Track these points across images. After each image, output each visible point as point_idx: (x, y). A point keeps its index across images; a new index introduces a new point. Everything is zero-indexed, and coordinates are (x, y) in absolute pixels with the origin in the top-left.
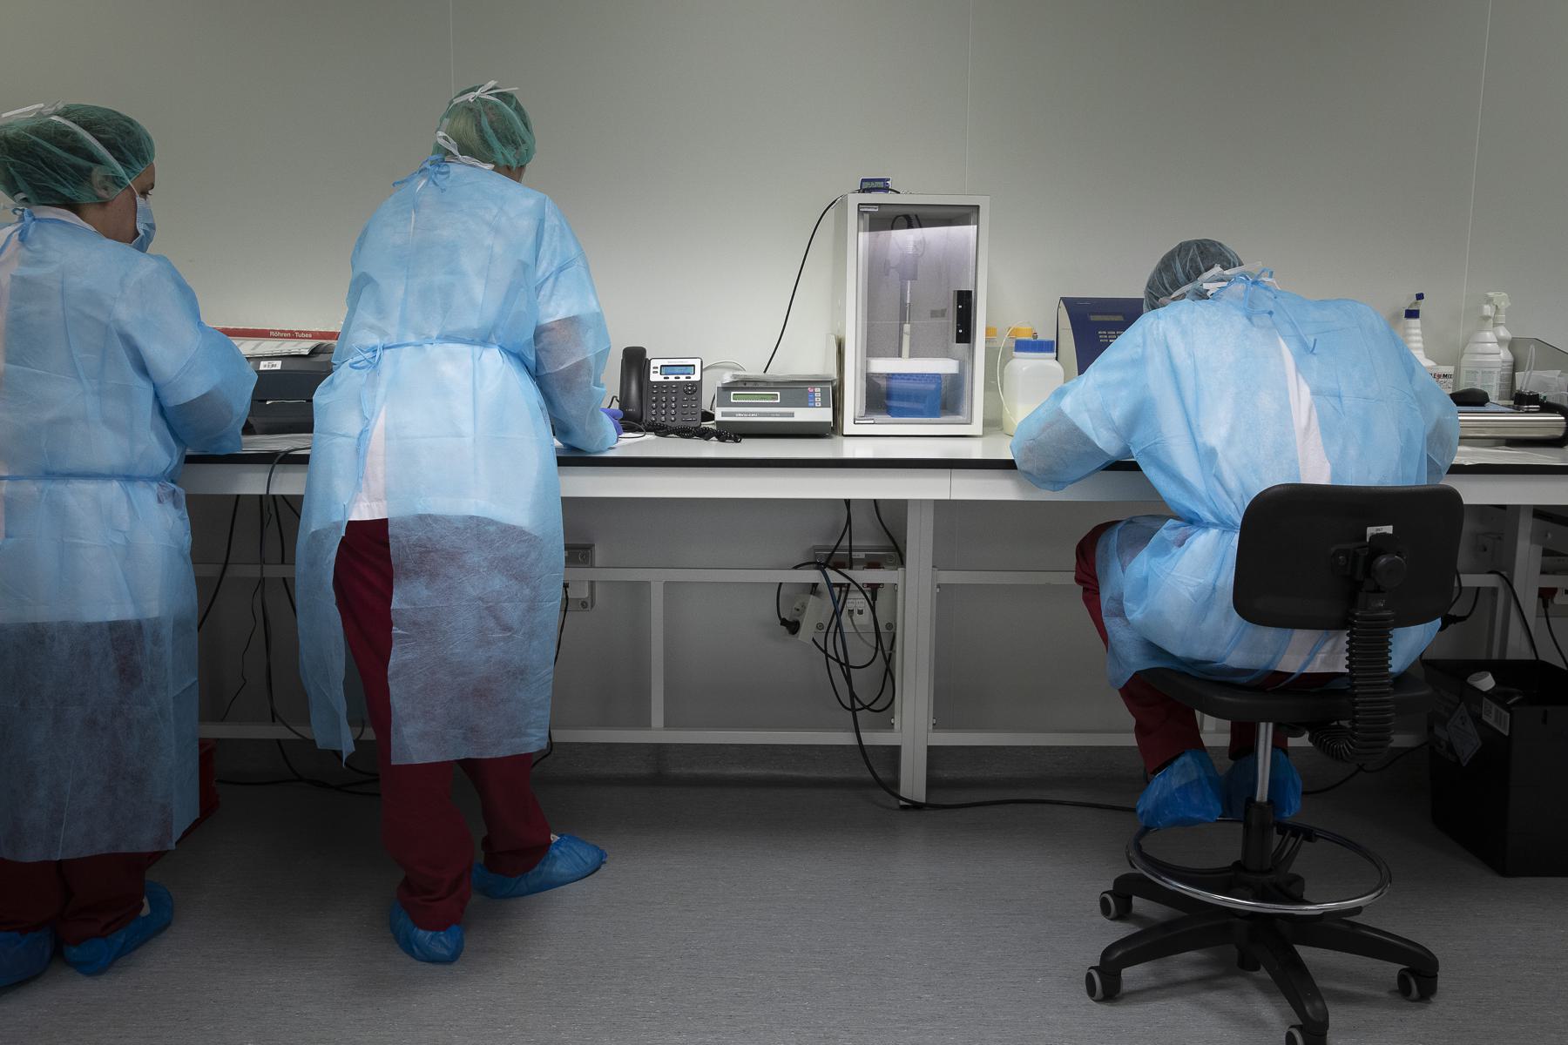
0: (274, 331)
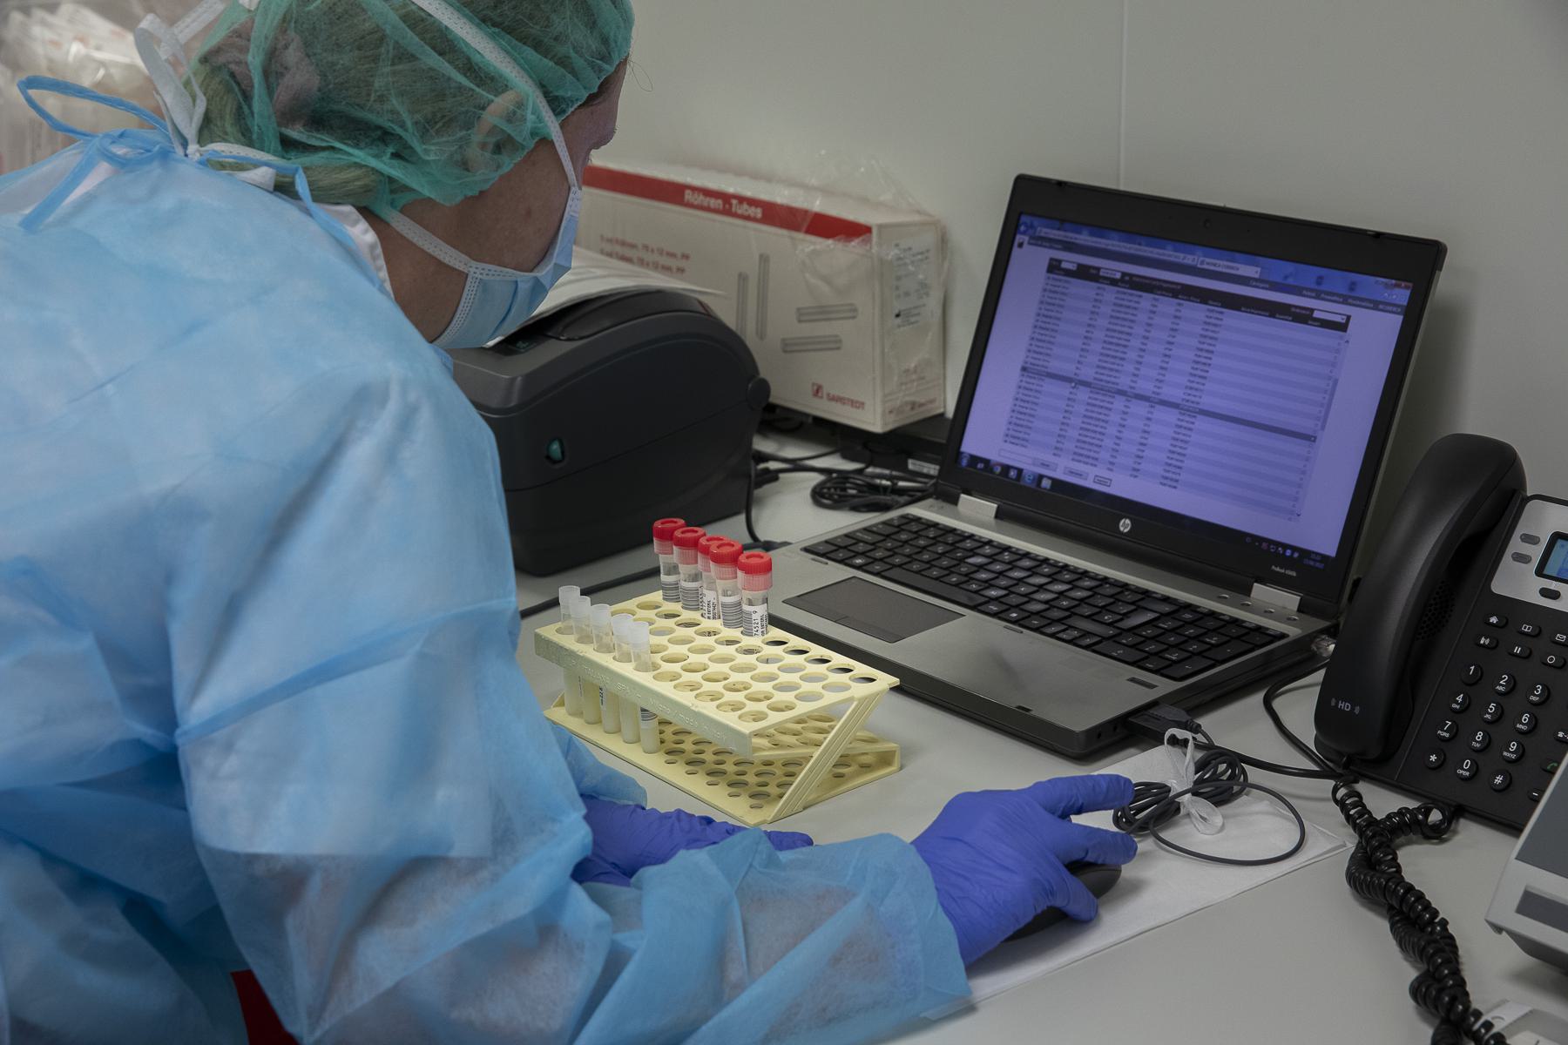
0: (694, 189)
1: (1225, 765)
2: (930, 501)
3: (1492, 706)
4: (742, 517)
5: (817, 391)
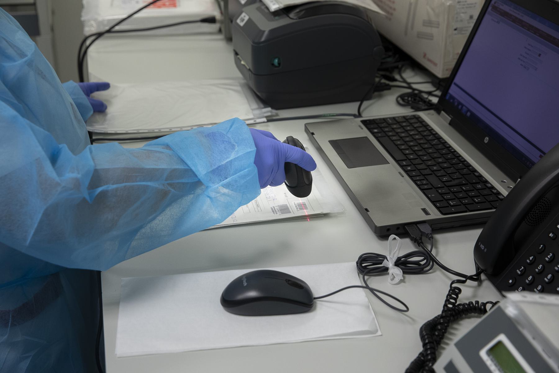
1: (424, 258)
2: (432, 112)
3: (541, 266)
4: (358, 103)
5: (425, 55)
